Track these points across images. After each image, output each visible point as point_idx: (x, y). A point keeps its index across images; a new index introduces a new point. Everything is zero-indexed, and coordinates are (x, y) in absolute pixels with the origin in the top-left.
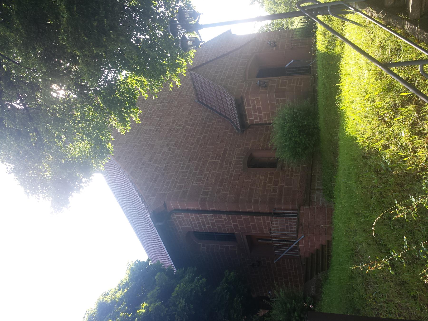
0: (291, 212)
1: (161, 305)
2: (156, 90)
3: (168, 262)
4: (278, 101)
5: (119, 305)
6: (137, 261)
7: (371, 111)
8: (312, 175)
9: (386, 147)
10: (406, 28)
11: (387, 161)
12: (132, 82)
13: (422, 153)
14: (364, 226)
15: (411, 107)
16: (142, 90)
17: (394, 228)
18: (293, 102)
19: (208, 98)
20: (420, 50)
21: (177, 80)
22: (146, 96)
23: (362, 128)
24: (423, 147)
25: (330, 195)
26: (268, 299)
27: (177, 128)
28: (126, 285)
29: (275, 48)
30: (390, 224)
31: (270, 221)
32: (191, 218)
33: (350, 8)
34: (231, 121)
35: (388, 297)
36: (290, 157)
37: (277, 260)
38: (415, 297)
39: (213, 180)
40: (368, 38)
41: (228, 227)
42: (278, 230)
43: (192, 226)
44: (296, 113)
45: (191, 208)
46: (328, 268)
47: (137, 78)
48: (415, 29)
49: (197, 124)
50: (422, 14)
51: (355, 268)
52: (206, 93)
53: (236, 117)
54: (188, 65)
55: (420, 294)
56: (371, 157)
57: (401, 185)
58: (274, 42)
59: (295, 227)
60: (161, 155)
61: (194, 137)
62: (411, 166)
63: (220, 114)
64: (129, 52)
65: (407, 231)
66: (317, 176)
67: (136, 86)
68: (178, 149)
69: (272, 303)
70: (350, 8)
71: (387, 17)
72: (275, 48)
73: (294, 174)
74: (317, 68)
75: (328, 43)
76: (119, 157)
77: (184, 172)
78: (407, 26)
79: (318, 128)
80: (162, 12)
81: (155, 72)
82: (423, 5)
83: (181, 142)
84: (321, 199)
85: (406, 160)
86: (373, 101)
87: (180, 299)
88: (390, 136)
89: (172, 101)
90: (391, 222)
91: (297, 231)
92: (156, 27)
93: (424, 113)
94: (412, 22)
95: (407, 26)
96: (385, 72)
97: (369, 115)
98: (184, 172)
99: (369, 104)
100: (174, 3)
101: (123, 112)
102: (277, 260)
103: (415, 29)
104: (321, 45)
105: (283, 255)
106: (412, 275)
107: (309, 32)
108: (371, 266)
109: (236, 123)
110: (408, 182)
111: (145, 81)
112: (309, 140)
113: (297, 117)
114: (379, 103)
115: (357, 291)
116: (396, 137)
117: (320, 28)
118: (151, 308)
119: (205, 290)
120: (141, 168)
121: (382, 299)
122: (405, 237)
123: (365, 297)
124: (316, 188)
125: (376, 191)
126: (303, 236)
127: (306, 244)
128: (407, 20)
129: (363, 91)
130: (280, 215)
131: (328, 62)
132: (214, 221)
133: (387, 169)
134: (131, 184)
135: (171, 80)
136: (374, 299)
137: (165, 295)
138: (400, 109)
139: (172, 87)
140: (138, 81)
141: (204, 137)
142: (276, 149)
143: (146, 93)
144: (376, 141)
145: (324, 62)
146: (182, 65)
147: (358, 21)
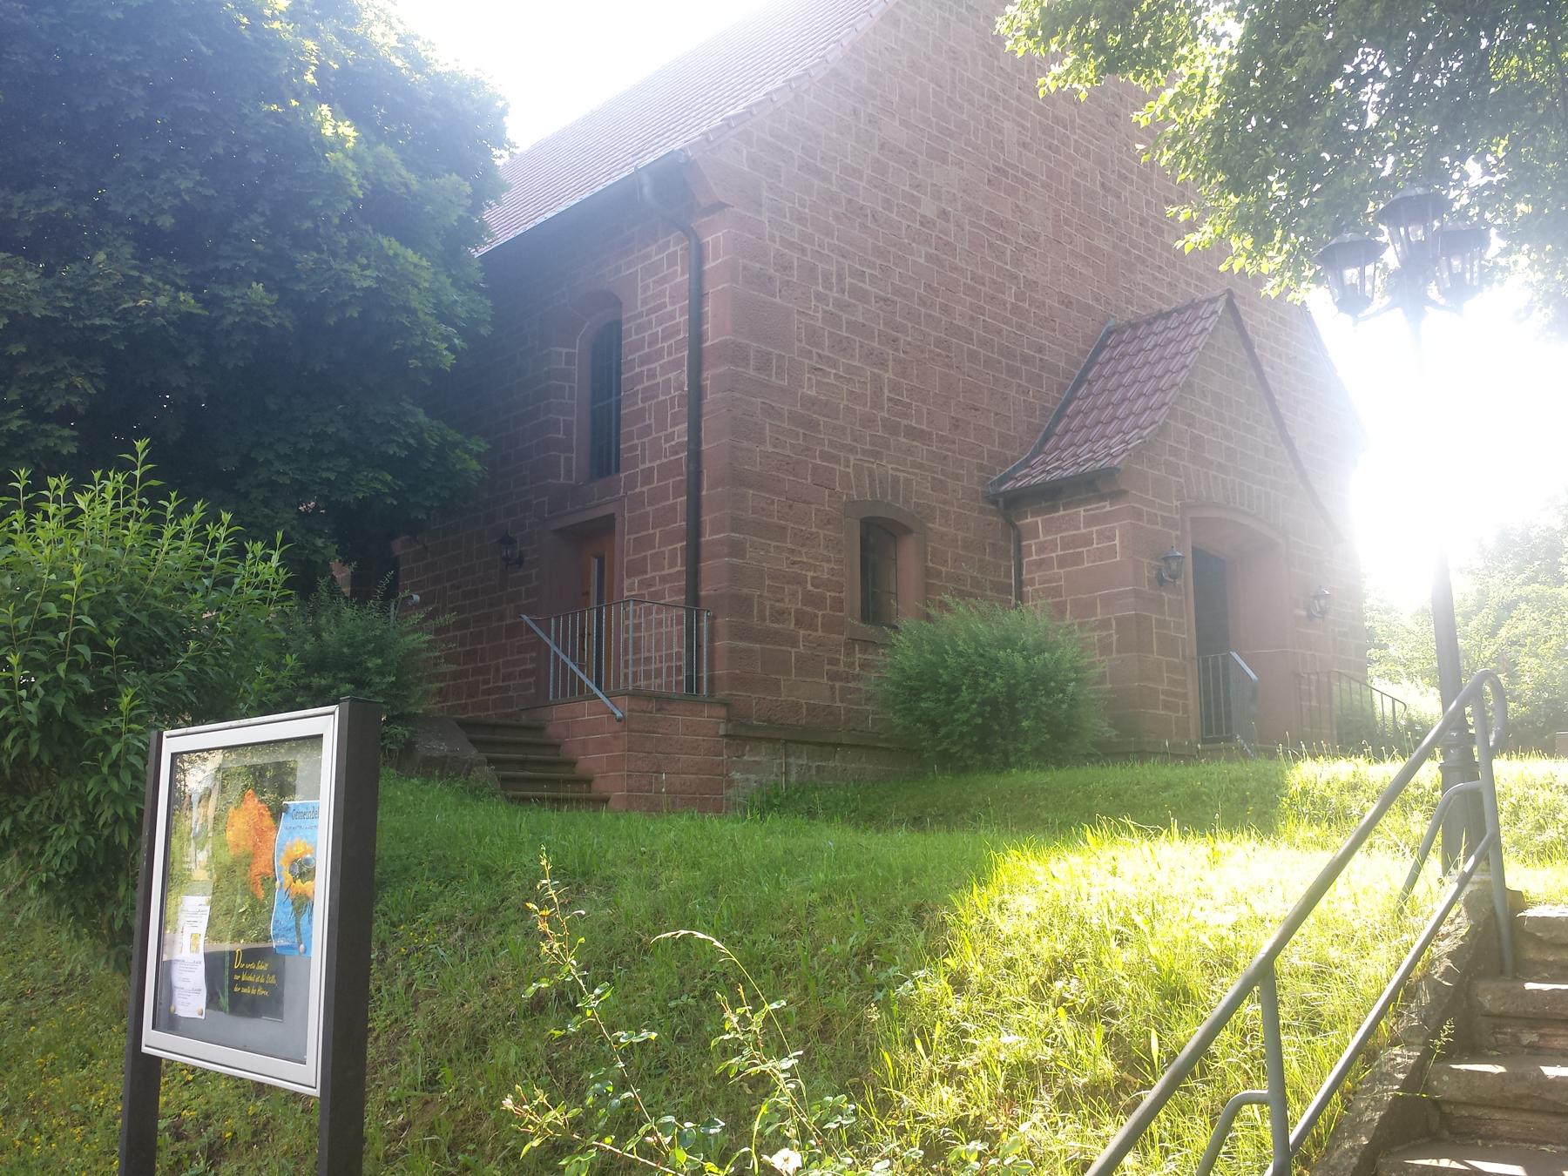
0: (704, 674)
1: (351, 198)
2: (1168, 155)
3: (505, 223)
4: (1104, 625)
5: (341, 35)
6: (507, 104)
7: (1087, 935)
8: (836, 745)
9: (959, 983)
10: (1397, 1050)
11: (909, 984)
12: (1198, 62)
13: (941, 1103)
14: (676, 911)
15: (1107, 1067)
16: (1167, 102)
17: (672, 1010)
18: (1101, 679)
19: (1120, 368)
20: (1316, 1100)
21: (1206, 237)
22: (1142, 118)
23: (1024, 902)
24: (963, 1107)
25: (771, 803)
26: (390, 593)
27: (1009, 249)
28: (419, 64)
29: (1303, 613)
30: (684, 998)
31: (667, 600)
32: (669, 308)
33: (1472, 859)
34: (1033, 456)
35: (430, 995)
36: (903, 670)
37: (533, 626)
38: (432, 1082)
39: (813, 393)
40: (1356, 925)
41: (643, 450)
42: (637, 628)
43: (641, 315)
44: (1063, 691)
45: (709, 308)
46: (512, 800)
47: (1215, 80)
48: (1393, 1081)
49: (1021, 327)
50: (1447, 1109)
51: (544, 863)
52: (1140, 358)
53: (1048, 472)
54: (1259, 280)
55: (446, 1099)
56: (922, 934)
57: (825, 1033)
58: (1323, 612)
59: (649, 686)
60: (907, 188)
61: (972, 318)
62: (896, 1064)
63: (1059, 416)
64: (1321, 40)
65: (663, 1054)
66: (831, 764)
67: (1181, 75)
68: (929, 257)
69: (381, 607)
70: (1472, 859)
71: (1436, 988)
72: (1303, 613)
73: (838, 684)
74: (1229, 760)
75: (1322, 798)
76: (896, 23)
77: (840, 278)
78: (1402, 1056)
79: (1007, 765)
80: (1465, 176)
81: (1234, 157)
82: (1478, 1112)
83: (954, 268)
84: (752, 777)
85: (915, 1050)
86: (1122, 942)
87: (378, 269)
88: (999, 995)
89: (1109, 231)
90: (692, 1001)
91: (636, 695)
92: (1408, 155)
93: (1086, 1110)
94: (1417, 1073)
95: (1403, 1057)
96: (1231, 984)
97: (1072, 926)
98: (840, 278)
99: (1115, 925)
100: (1499, 221)
101: (1081, 25)
102: (533, 626)
103: (1393, 1081)
104: (1311, 774)
105: (551, 644)
106: (511, 1071)
107: (1358, 734)
108: (549, 920)
109: (1026, 476)
110: (838, 1055)
111: (1203, 112)
112: (962, 735)
113: (1048, 694)
114: (1119, 960)
115: (442, 893)
116: (997, 1019)
117: (1388, 771)
118: (337, 161)
119: (413, 363)
120: (855, 112)
121: (418, 974)
122: (654, 1035)
123: (423, 918)
124: (792, 760)
125: (799, 950)
126: (619, 715)
127: (591, 724)
128: (1427, 1053)
129: (1158, 907)
130: (692, 634)
131: (1252, 797)
132: (662, 398)
133: (880, 987)
134: (795, 72)
135: (1206, 212)
136: (418, 949)
137: (387, 211)
138: (1098, 1031)
139: (1182, 218)
140: (1203, 86)
141: (973, 356)
142: (929, 618)
143: (1154, 117)
144: (980, 951)
145: (1252, 784)
146: (1262, 255)
147: (1419, 889)
